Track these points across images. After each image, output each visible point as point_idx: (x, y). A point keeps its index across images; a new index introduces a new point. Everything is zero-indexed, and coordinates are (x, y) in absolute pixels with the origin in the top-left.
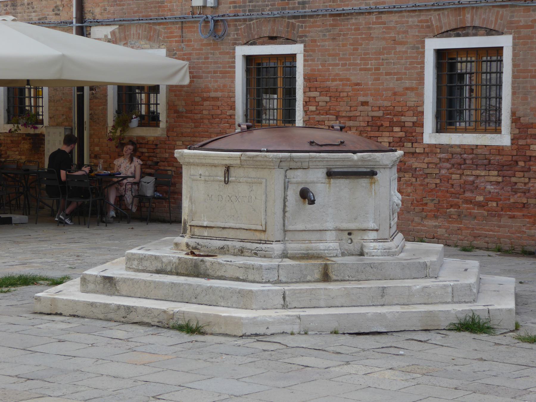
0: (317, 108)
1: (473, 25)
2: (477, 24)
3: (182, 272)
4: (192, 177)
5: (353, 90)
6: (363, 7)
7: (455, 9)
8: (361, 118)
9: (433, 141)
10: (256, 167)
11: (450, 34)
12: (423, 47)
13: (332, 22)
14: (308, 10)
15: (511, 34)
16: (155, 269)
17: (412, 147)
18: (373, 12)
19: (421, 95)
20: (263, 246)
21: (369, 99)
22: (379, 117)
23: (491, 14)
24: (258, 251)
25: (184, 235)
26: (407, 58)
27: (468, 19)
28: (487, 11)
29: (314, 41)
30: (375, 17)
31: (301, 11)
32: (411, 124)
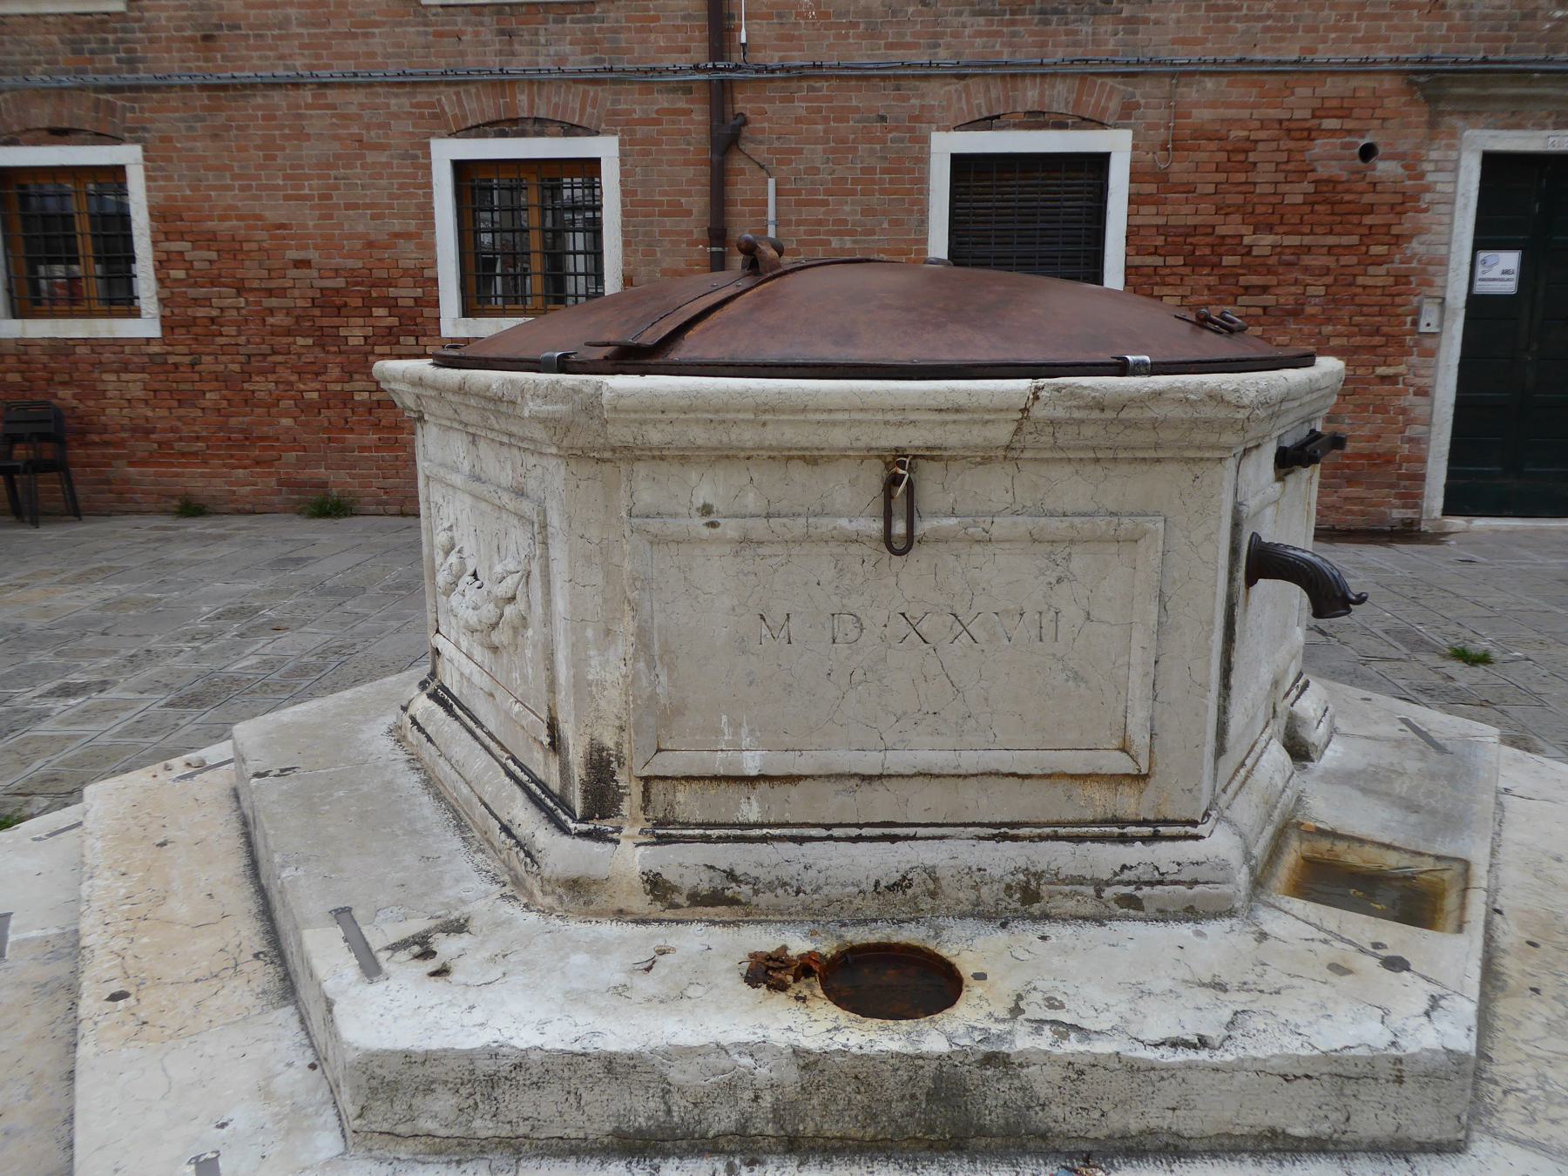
0: (187, 274)
1: (535, 115)
2: (542, 114)
3: (832, 1129)
4: (654, 525)
5: (273, 237)
6: (280, 72)
7: (493, 84)
8: (296, 293)
9: (462, 333)
10: (1103, 458)
11: (485, 131)
12: (428, 155)
13: (206, 102)
14: (144, 77)
15: (615, 134)
16: (608, 1127)
17: (417, 344)
18: (305, 84)
19: (430, 247)
20: (1165, 854)
21: (313, 255)
22: (337, 291)
23: (571, 97)
24: (1139, 884)
25: (606, 825)
26: (391, 176)
27: (523, 103)
28: (563, 90)
29: (166, 139)
30: (309, 93)
31: (126, 76)
32: (411, 303)
